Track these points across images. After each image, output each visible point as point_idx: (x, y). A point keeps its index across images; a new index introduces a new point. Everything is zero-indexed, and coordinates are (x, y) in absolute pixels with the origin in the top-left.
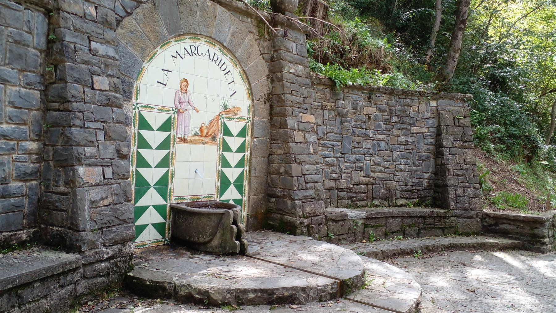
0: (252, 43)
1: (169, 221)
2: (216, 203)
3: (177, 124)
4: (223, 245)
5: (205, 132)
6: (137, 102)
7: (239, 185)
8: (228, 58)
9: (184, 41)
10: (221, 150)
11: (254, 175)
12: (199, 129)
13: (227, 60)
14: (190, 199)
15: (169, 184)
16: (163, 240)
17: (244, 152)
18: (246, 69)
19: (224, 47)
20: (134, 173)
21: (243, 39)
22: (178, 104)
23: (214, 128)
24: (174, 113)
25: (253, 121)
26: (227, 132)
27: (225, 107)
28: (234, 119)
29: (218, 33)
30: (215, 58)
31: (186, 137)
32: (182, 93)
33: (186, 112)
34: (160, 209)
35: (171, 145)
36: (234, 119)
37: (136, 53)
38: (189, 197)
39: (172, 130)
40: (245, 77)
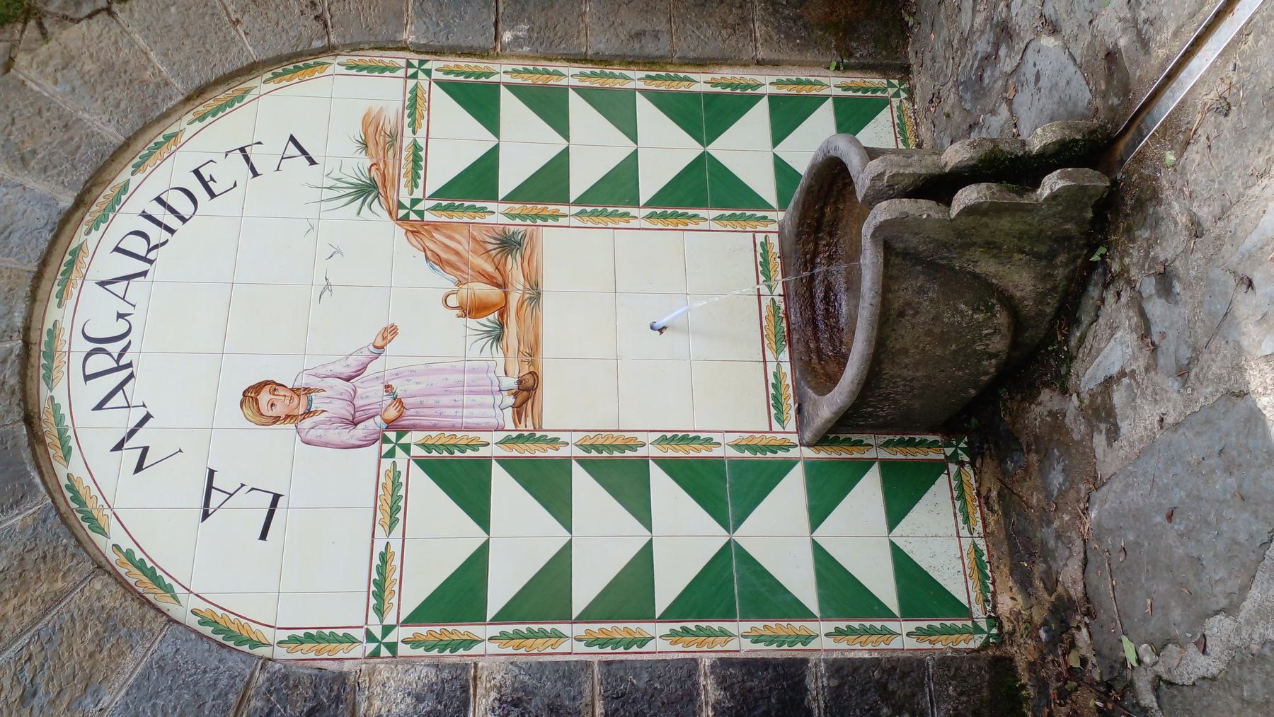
0: (57, 61)
1: (876, 448)
2: (799, 235)
3: (453, 428)
4: (1043, 249)
5: (483, 290)
6: (359, 634)
7: (706, 116)
8: (135, 181)
9: (64, 410)
10: (563, 209)
11: (665, 38)
12: (472, 323)
13: (144, 187)
14: (778, 352)
15: (717, 452)
16: (953, 468)
17: (565, 90)
18: (179, 88)
19: (81, 202)
20: (677, 626)
21: (41, 106)
22: (360, 431)
23: (463, 246)
24: (406, 448)
25: (418, 49)
26: (478, 180)
27: (366, 190)
28: (416, 147)
29: (15, 239)
30: (139, 246)
31: (511, 382)
32: (308, 413)
33: (400, 387)
34: (825, 495)
35: (551, 453)
36: (416, 147)
37: (132, 665)
38: (770, 355)
39: (483, 452)
40: (222, 94)
